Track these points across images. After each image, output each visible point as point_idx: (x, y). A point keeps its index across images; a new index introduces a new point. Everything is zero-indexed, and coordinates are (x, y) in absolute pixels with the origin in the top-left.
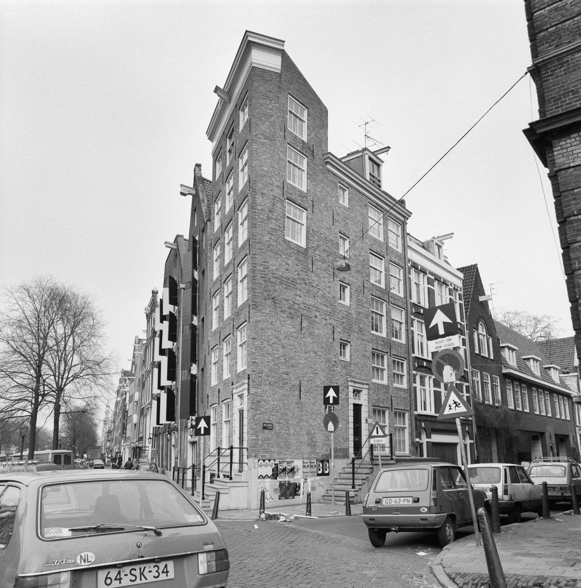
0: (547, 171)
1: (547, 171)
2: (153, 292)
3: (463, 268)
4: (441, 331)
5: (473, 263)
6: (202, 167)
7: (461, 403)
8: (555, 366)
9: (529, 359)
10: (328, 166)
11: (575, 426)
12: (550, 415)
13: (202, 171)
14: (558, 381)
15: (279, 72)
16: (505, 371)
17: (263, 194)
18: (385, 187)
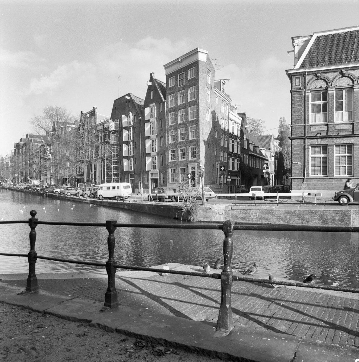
5: (244, 112)
10: (215, 91)
12: (260, 168)
16: (250, 153)
17: (202, 106)
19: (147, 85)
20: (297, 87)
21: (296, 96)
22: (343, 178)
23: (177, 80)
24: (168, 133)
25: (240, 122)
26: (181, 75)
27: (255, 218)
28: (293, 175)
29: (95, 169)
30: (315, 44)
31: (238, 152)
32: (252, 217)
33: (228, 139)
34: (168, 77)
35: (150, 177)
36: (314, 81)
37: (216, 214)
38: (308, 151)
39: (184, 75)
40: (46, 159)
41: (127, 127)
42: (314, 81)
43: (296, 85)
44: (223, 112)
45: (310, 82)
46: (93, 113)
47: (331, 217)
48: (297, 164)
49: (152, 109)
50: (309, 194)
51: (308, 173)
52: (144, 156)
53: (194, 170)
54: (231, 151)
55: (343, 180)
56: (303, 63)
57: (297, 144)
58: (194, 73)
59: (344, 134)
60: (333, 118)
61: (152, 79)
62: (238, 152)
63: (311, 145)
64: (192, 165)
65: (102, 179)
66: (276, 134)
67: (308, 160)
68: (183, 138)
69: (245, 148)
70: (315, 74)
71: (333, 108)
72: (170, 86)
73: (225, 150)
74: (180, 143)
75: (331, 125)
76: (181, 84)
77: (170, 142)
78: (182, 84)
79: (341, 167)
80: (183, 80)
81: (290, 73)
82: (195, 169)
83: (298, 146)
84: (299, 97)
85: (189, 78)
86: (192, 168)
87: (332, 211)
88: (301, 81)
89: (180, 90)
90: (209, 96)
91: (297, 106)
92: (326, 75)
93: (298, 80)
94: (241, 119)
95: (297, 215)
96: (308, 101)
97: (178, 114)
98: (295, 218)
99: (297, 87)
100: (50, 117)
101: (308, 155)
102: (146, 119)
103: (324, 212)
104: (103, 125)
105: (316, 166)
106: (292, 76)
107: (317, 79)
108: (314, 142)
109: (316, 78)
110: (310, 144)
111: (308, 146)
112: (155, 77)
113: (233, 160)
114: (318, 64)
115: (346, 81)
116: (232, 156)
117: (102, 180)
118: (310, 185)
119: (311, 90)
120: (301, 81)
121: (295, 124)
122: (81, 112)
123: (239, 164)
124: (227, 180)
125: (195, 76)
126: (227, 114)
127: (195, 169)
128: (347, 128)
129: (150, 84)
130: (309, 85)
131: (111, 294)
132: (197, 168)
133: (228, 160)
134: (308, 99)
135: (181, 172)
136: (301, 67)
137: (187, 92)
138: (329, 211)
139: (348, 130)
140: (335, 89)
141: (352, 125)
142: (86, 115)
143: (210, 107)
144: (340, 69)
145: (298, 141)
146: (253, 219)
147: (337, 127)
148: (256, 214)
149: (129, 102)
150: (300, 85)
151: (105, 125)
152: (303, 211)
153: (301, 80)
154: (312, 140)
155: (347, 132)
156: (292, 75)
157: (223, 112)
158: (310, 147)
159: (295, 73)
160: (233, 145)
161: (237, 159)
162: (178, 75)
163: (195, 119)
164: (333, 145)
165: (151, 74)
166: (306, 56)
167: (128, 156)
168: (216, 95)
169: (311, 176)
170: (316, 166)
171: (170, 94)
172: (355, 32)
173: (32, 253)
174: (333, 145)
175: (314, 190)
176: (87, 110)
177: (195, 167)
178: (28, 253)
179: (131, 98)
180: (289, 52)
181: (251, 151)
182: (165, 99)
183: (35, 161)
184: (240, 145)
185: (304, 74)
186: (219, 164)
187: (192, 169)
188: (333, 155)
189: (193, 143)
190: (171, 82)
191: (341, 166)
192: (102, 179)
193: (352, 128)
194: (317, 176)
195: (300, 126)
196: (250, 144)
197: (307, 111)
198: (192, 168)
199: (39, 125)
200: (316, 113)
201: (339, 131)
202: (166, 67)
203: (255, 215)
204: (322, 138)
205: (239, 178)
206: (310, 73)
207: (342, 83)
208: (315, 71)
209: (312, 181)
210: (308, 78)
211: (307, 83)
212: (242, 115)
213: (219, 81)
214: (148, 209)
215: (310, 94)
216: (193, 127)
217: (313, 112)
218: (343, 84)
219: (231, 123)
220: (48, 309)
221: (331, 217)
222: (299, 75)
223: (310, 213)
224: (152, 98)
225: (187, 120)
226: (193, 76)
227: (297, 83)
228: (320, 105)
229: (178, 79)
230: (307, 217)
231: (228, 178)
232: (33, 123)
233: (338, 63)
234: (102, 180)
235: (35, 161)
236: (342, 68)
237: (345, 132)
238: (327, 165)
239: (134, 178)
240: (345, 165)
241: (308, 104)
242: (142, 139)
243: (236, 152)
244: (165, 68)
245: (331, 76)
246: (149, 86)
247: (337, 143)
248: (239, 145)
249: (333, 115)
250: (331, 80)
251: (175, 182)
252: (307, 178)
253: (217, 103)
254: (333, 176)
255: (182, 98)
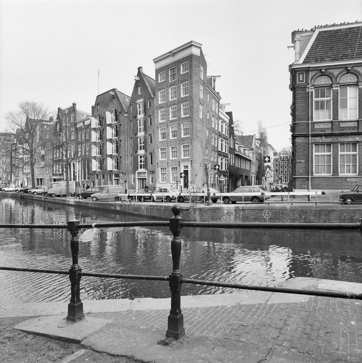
0: (292, 133)
1: (292, 133)
2: (73, 104)
3: (228, 112)
4: (267, 161)
5: (231, 111)
6: (143, 68)
7: (358, 193)
8: (238, 143)
9: (241, 147)
10: (207, 88)
11: (250, 172)
12: (239, 167)
13: (143, 70)
14: (243, 152)
15: (199, 56)
16: (236, 153)
17: (196, 103)
18: (216, 90)
19: (135, 80)
20: (301, 83)
21: (299, 92)
22: (347, 176)
23: (168, 75)
24: (158, 130)
25: (227, 121)
26: (172, 70)
27: (268, 218)
28: (297, 174)
29: (74, 168)
30: (317, 39)
31: (226, 151)
32: (265, 217)
33: (218, 137)
34: (158, 71)
35: (137, 177)
36: (318, 77)
37: (225, 214)
38: (312, 149)
39: (176, 70)
40: (17, 158)
41: (111, 124)
42: (318, 77)
43: (299, 81)
44: (214, 110)
45: (314, 78)
46: (73, 109)
47: (350, 217)
48: (301, 162)
49: (139, 105)
50: (323, 193)
51: (312, 172)
52: (130, 155)
53: (186, 169)
54: (220, 150)
55: (348, 179)
56: (306, 58)
57: (300, 141)
58: (188, 68)
59: (349, 132)
60: (338, 115)
61: (140, 74)
62: (226, 151)
63: (315, 143)
64: (185, 164)
65: (82, 179)
66: (258, 136)
67: (312, 159)
68: (174, 136)
69: (232, 147)
70: (319, 69)
71: (338, 105)
72: (159, 82)
73: (215, 149)
74: (183, 139)
75: (335, 123)
76: (172, 79)
77: (160, 140)
78: (174, 79)
79: (345, 165)
80: (175, 75)
81: (294, 69)
82: (188, 168)
83: (302, 144)
84: (303, 93)
85: (182, 73)
86: (185, 166)
87: (350, 210)
88: (305, 77)
89: (172, 85)
90: (202, 92)
91: (300, 103)
92: (331, 71)
93: (301, 76)
94: (229, 118)
95: (313, 214)
96: (312, 98)
97: (169, 111)
98: (311, 218)
99: (301, 83)
100: (26, 112)
101: (312, 153)
102: (107, 123)
103: (342, 211)
104: (84, 123)
105: (326, 164)
106: (295, 71)
107: (321, 75)
108: (318, 139)
109: (320, 74)
110: (313, 141)
111: (312, 144)
112: (145, 71)
113: (222, 159)
114: (322, 60)
115: (351, 78)
116: (221, 156)
117: (83, 180)
118: (314, 184)
119: (315, 86)
120: (305, 77)
121: (299, 121)
122: (59, 109)
123: (226, 164)
124: (220, 180)
125: (188, 71)
126: (217, 112)
127: (188, 168)
128: (352, 126)
129: (138, 79)
130: (313, 81)
131: (178, 318)
132: (189, 167)
133: (217, 159)
134: (312, 96)
135: (172, 171)
136: (304, 63)
137: (179, 87)
138: (347, 210)
139: (353, 128)
140: (340, 85)
141: (356, 123)
142: (65, 111)
143: (203, 104)
144: (345, 65)
145: (302, 138)
146: (265, 219)
147: (342, 125)
148: (268, 214)
149: (114, 98)
150: (303, 81)
151: (86, 122)
152: (319, 210)
153: (305, 75)
154: (316, 138)
155: (352, 129)
156: (296, 70)
157: (214, 110)
158: (314, 145)
159: (299, 68)
160: (222, 144)
161: (221, 157)
162: (169, 70)
163: (189, 115)
164: (338, 143)
165: (139, 68)
166: (309, 51)
167: (112, 155)
168: (207, 92)
169: (315, 175)
170: (320, 164)
171: (160, 90)
172: (359, 27)
173: (75, 268)
174: (338, 143)
175: (318, 189)
176: (66, 105)
177: (188, 166)
178: (70, 270)
179: (116, 94)
180: (289, 47)
181: (237, 151)
182: (155, 95)
183: (6, 161)
184: (228, 144)
185: (307, 70)
186: (210, 164)
187: (185, 168)
188: (338, 153)
189: (186, 141)
190: (161, 77)
191: (345, 164)
192: (82, 179)
193: (357, 126)
194: (321, 174)
195: (304, 123)
196: (236, 144)
197: (311, 107)
198: (185, 166)
199: (13, 121)
200: (320, 110)
201: (343, 128)
202: (156, 61)
203: (268, 215)
204: (327, 135)
205: (227, 178)
206: (314, 69)
207: (347, 79)
208: (320, 67)
209: (316, 180)
210: (311, 74)
211: (311, 79)
212: (230, 114)
213: (211, 77)
214: (145, 209)
215: (314, 90)
216: (186, 124)
217: (317, 108)
218: (348, 81)
219: (220, 121)
220: (24, 319)
221: (350, 217)
222: (303, 71)
223: (327, 213)
224: (139, 94)
225: (179, 117)
226: (185, 71)
227: (301, 79)
228: (324, 101)
229: (170, 74)
230: (323, 217)
231: (221, 177)
232: (7, 118)
233: (342, 59)
234: (83, 180)
235: (6, 161)
236: (347, 64)
237: (350, 129)
238: (331, 163)
239: (118, 178)
240: (350, 163)
241: (312, 100)
242: (128, 137)
243: (224, 151)
244: (155, 62)
245: (336, 72)
246: (137, 82)
247: (342, 141)
248: (227, 144)
249: (338, 111)
250: (336, 76)
251: (165, 182)
252: (312, 177)
253: (208, 100)
254: (338, 175)
255: (163, 98)
